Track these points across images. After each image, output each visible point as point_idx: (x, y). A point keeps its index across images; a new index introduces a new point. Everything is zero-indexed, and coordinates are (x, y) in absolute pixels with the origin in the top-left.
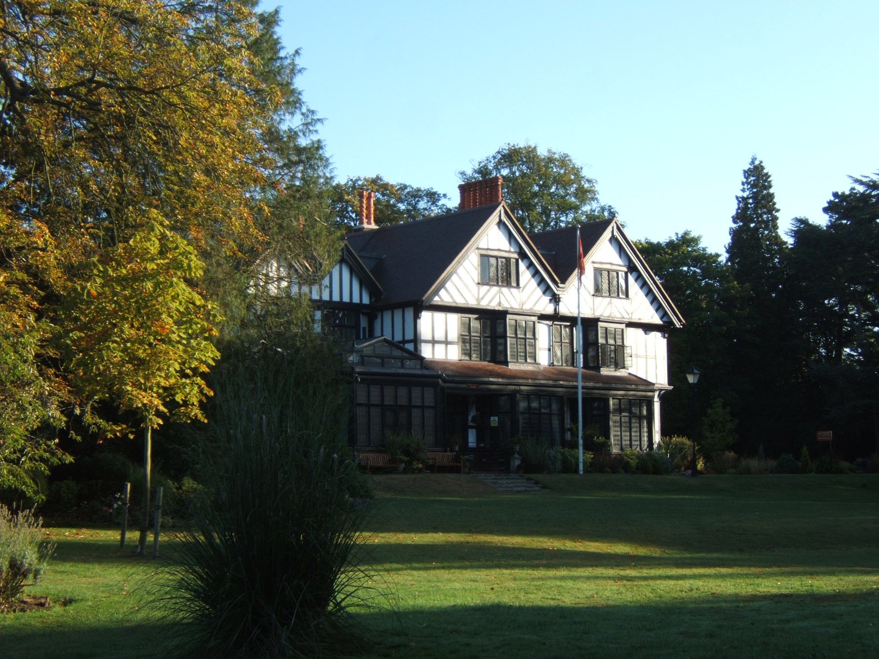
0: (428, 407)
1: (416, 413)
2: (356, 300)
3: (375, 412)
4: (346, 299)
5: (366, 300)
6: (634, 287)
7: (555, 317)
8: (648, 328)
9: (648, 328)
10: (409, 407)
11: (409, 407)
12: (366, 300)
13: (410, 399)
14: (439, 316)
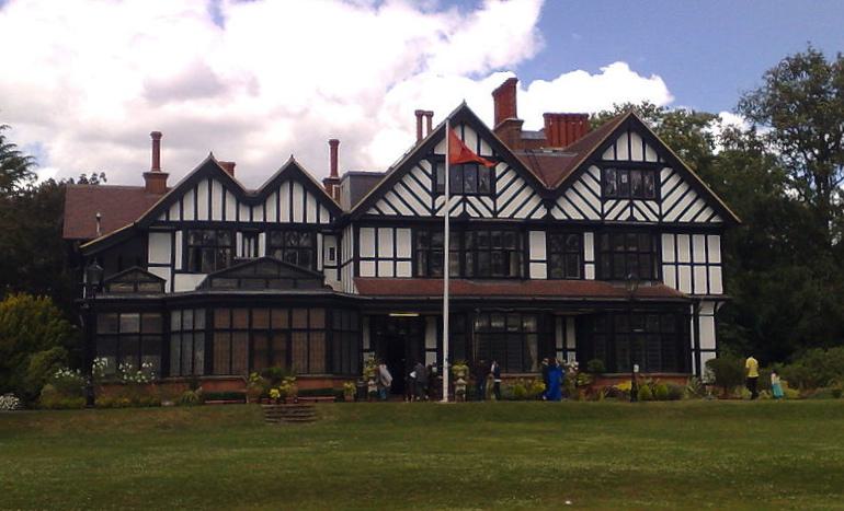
2: (311, 219)
4: (298, 219)
5: (325, 219)
7: (547, 225)
8: (692, 229)
9: (692, 229)
10: (288, 333)
11: (288, 333)
12: (325, 219)
14: (386, 234)
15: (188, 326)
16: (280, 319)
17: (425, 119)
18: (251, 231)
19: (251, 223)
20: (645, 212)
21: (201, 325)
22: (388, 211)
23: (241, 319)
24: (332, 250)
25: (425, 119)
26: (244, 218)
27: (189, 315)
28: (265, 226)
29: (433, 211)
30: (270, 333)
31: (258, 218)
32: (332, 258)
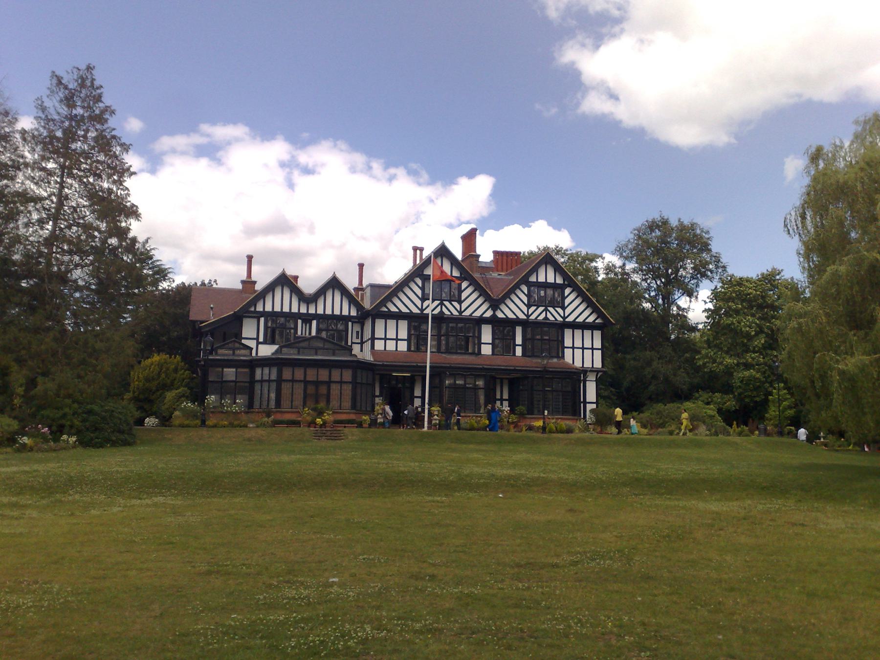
0: (346, 382)
1: (335, 388)
2: (345, 312)
3: (299, 389)
4: (337, 312)
5: (354, 313)
6: (468, 291)
7: (493, 321)
10: (329, 383)
11: (329, 383)
12: (354, 313)
13: (330, 376)
14: (391, 323)
15: (266, 378)
16: (324, 374)
17: (418, 252)
18: (307, 319)
19: (308, 314)
20: (555, 315)
21: (274, 377)
22: (393, 309)
23: (299, 374)
24: (358, 332)
25: (418, 252)
26: (303, 310)
27: (266, 370)
28: (316, 316)
29: (564, 318)
30: (317, 383)
31: (312, 311)
32: (357, 338)
